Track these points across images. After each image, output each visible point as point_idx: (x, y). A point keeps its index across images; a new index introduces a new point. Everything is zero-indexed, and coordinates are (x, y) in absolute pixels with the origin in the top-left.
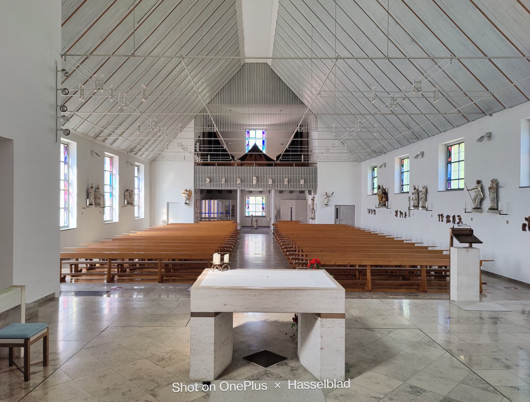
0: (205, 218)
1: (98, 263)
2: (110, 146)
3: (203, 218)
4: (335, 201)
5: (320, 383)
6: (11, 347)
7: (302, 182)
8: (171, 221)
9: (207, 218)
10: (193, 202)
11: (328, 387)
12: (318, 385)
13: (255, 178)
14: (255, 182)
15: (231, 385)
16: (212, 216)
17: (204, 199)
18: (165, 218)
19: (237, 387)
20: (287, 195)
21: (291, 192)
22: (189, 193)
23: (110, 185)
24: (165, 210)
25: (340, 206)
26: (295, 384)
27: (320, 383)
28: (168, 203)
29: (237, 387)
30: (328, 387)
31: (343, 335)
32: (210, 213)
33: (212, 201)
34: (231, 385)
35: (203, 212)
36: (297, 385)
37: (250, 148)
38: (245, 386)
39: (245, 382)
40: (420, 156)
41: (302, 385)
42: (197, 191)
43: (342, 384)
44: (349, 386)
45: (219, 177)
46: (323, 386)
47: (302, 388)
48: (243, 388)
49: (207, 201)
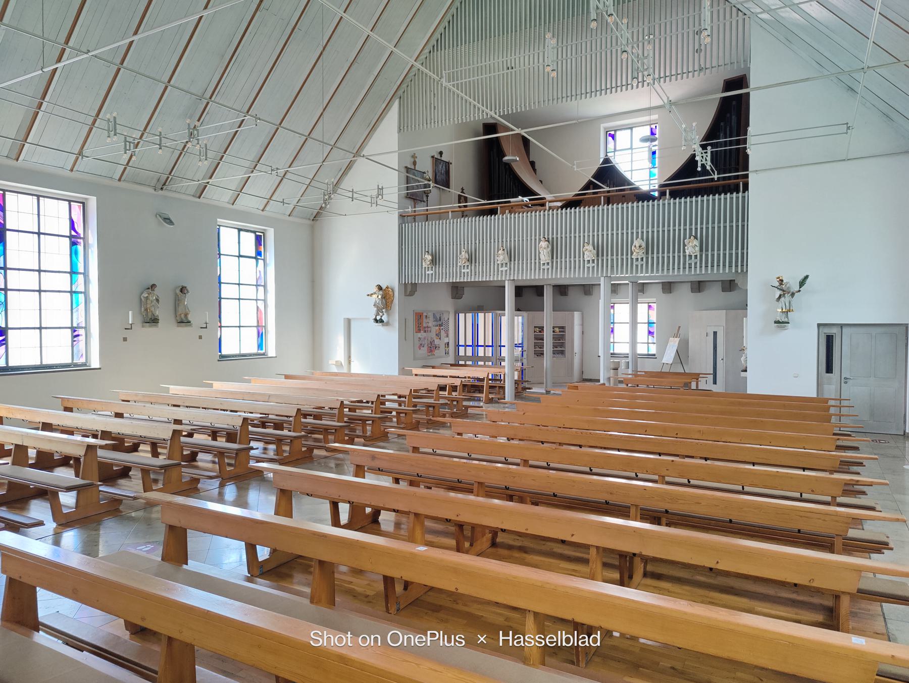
0: (466, 358)
1: (207, 450)
2: (13, 163)
3: (462, 358)
4: (811, 314)
5: (552, 638)
6: (837, 597)
7: (692, 247)
8: (357, 368)
9: (469, 358)
10: (396, 316)
11: (564, 644)
12: (547, 640)
13: (544, 244)
14: (545, 256)
15: (406, 637)
16: (481, 354)
17: (466, 311)
18: (339, 354)
19: (416, 640)
20: (684, 293)
21: (698, 286)
22: (385, 295)
23: (84, 274)
24: (341, 340)
25: (842, 326)
26: (510, 638)
27: (552, 638)
28: (349, 322)
29: (416, 640)
30: (564, 644)
31: (788, 580)
32: (475, 345)
33: (481, 315)
34: (406, 637)
35: (462, 342)
36: (514, 640)
37: (601, 160)
38: (429, 639)
39: (429, 632)
40: (411, 166)
41: (522, 639)
42: (409, 290)
43: (587, 639)
44: (599, 644)
45: (514, 245)
46: (557, 642)
47: (522, 644)
48: (426, 642)
49: (469, 316)
